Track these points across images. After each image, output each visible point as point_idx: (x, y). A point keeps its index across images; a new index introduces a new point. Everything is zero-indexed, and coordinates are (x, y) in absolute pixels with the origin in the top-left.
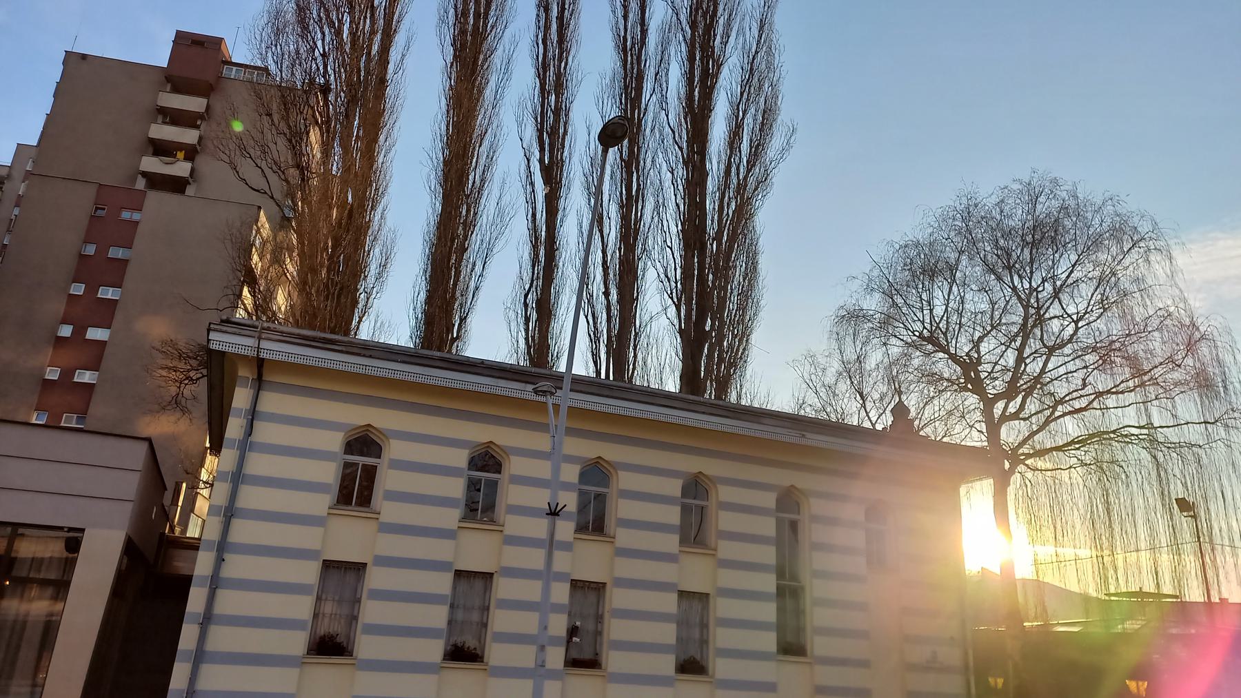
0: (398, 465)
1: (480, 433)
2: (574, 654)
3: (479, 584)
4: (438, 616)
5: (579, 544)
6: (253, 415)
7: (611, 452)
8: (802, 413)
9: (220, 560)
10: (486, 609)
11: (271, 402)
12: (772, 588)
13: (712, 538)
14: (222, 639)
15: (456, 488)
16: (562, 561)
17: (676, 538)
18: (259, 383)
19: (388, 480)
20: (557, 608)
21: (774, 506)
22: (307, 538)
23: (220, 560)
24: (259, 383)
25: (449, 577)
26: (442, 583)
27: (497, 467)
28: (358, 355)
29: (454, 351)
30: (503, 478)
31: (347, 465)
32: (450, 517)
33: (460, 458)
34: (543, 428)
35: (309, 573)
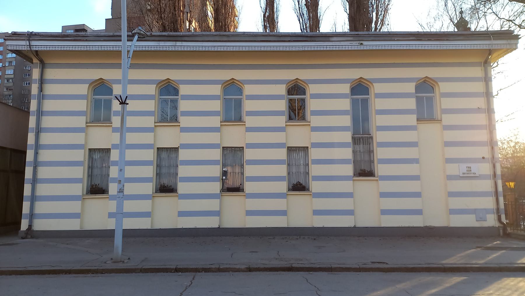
0: (252, 97)
1: (291, 75)
2: (226, 186)
3: (302, 154)
4: (282, 170)
5: (224, 128)
6: (42, 81)
7: (302, 75)
8: (503, 29)
9: (36, 154)
10: (242, 166)
11: (51, 74)
12: (349, 140)
13: (438, 113)
14: (42, 190)
15: (282, 105)
16: (116, 138)
17: (414, 117)
18: (43, 65)
19: (312, 105)
20: (115, 163)
21: (414, 92)
22: (213, 138)
23: (36, 154)
24: (43, 65)
25: (285, 151)
26: (282, 154)
27: (366, 91)
28: (310, 41)
29: (232, 31)
30: (307, 97)
31: (290, 100)
32: (281, 121)
33: (282, 89)
34: (118, 66)
35: (216, 154)
